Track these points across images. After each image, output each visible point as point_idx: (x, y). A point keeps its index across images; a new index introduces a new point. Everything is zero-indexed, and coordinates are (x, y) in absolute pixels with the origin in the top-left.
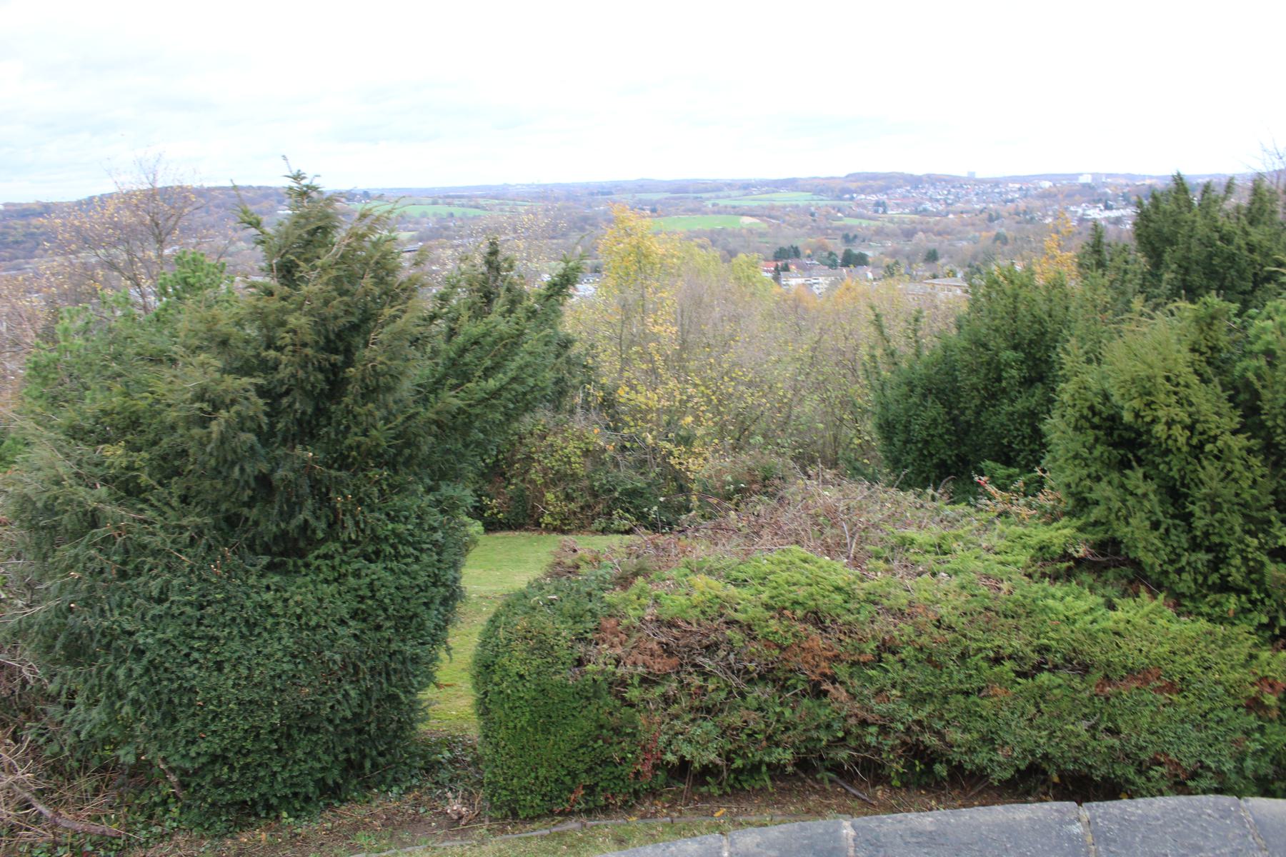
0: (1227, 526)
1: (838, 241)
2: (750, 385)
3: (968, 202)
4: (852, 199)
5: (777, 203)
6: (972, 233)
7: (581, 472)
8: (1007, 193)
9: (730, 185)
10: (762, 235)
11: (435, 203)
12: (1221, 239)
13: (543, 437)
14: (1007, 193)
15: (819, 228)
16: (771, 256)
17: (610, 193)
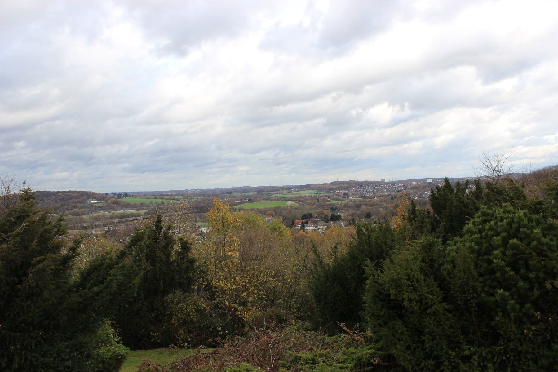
0: (440, 346)
1: (329, 210)
2: (274, 277)
3: (383, 192)
4: (334, 192)
5: (302, 195)
6: (385, 205)
7: (195, 320)
8: (398, 187)
9: (283, 188)
10: (296, 209)
11: (156, 198)
12: (464, 206)
13: (178, 304)
14: (398, 187)
15: (320, 205)
16: (300, 218)
17: (231, 193)
